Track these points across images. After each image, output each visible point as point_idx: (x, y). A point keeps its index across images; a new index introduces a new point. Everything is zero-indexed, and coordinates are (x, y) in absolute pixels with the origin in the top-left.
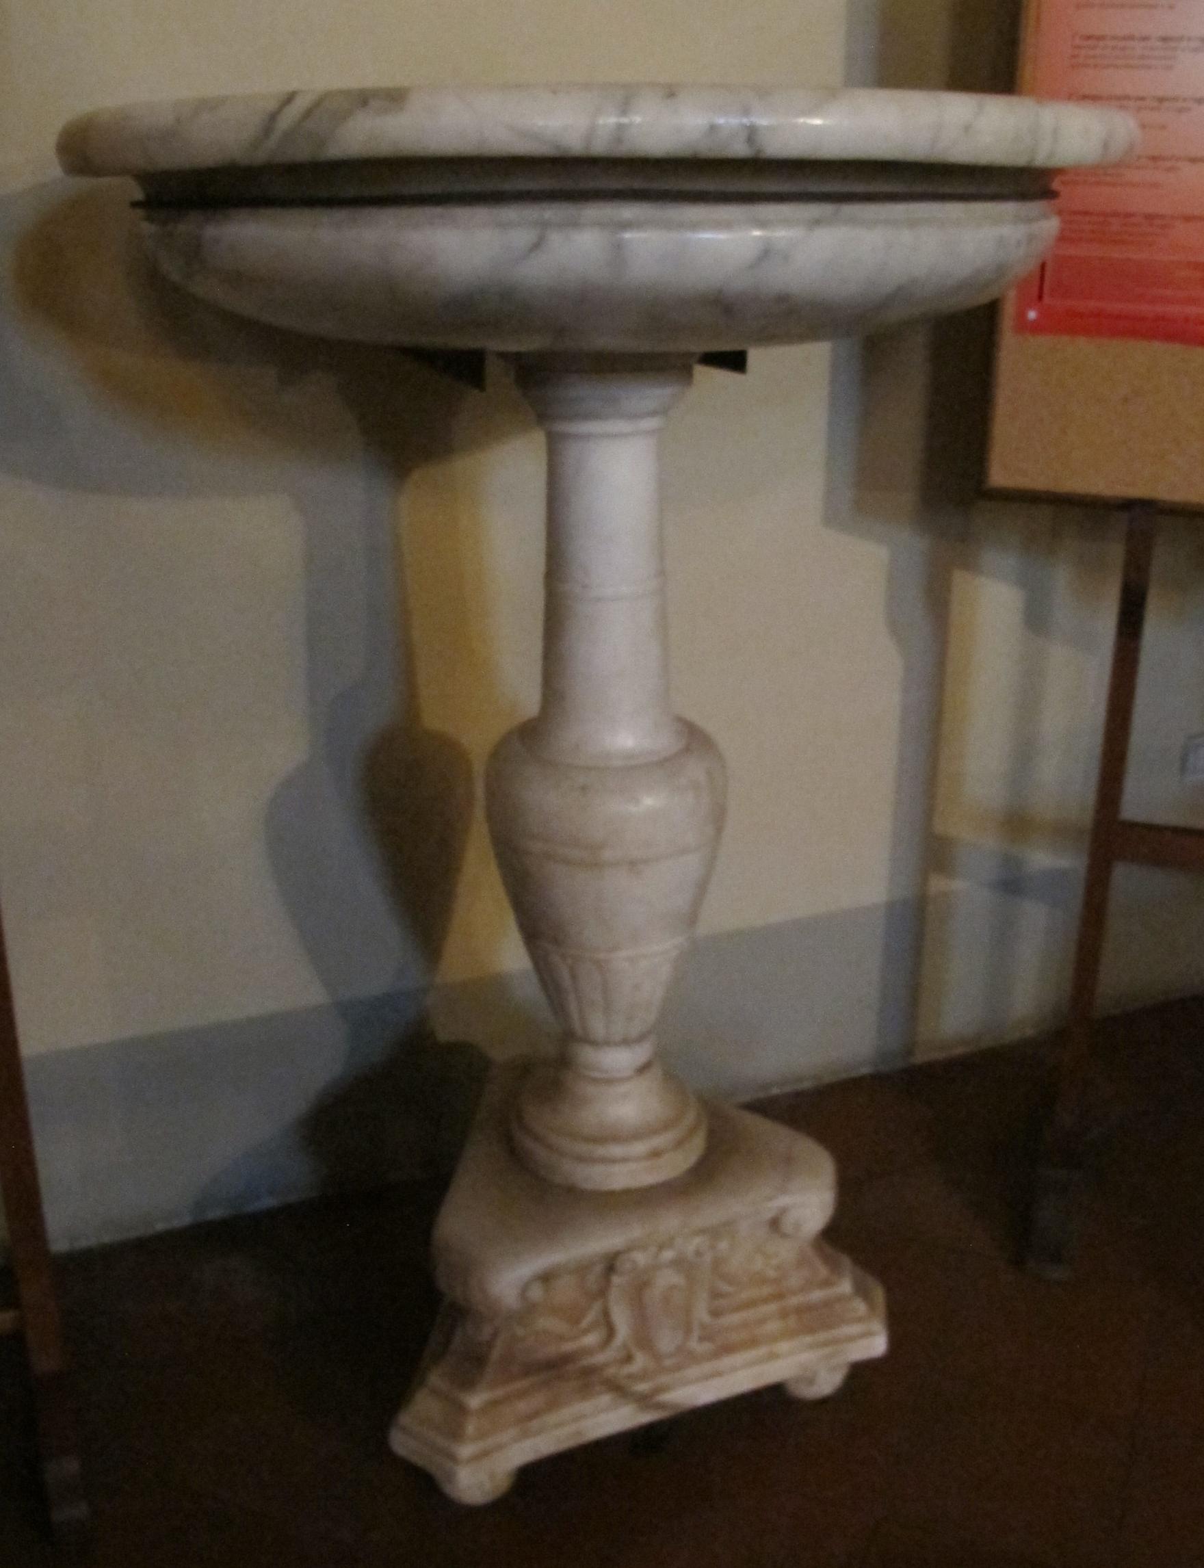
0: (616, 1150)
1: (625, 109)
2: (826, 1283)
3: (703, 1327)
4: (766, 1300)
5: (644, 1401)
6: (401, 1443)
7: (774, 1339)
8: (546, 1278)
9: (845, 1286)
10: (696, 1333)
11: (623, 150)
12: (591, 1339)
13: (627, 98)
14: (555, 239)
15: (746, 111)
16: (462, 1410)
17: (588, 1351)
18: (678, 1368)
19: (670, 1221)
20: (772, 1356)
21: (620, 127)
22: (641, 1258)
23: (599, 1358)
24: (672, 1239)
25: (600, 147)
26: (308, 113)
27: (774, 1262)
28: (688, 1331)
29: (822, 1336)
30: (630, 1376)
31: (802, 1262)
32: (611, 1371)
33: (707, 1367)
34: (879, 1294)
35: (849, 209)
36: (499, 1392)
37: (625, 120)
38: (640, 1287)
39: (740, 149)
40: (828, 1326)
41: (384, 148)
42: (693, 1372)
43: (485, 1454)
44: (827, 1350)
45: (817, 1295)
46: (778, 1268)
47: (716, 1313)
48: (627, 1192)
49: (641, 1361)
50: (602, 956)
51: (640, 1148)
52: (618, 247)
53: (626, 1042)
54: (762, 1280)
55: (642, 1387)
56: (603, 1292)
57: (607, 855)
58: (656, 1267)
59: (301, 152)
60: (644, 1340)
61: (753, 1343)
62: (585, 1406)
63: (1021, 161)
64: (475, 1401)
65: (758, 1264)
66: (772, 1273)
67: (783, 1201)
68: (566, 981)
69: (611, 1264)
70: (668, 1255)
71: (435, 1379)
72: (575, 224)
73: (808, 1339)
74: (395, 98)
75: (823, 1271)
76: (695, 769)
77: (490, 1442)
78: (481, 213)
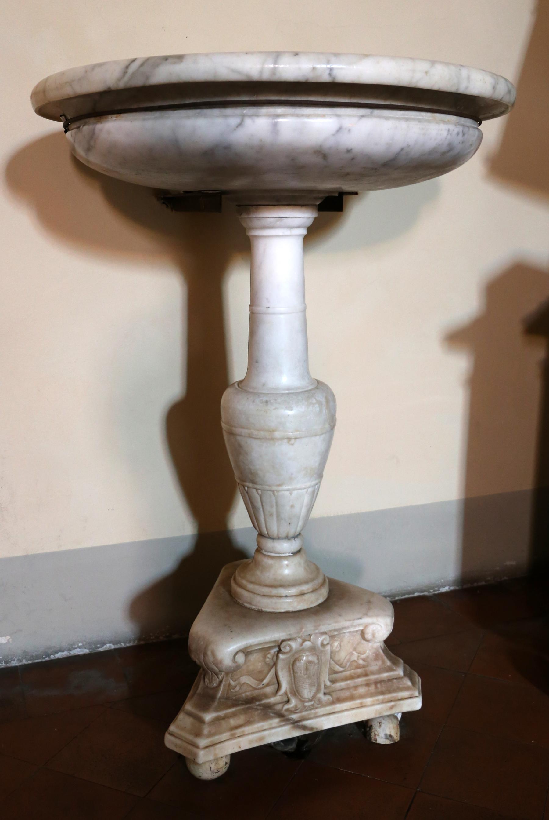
0: (283, 592)
1: (275, 62)
2: (390, 670)
3: (326, 687)
4: (359, 676)
5: (295, 724)
6: (170, 741)
7: (362, 697)
8: (246, 652)
9: (400, 672)
10: (323, 690)
11: (275, 78)
12: (269, 690)
13: (277, 56)
14: (248, 122)
15: (328, 62)
16: (201, 721)
17: (266, 696)
18: (313, 707)
19: (309, 626)
20: (362, 706)
21: (275, 69)
22: (294, 645)
23: (272, 700)
24: (310, 635)
25: (266, 77)
26: (142, 65)
27: (363, 656)
28: (318, 691)
29: (388, 696)
30: (287, 710)
31: (377, 657)
32: (279, 707)
33: (329, 709)
34: (418, 680)
35: (377, 112)
36: (222, 713)
37: (276, 66)
38: (292, 665)
39: (325, 78)
40: (390, 692)
41: (174, 79)
42: (321, 711)
43: (213, 745)
44: (392, 704)
45: (385, 675)
46: (364, 660)
47: (333, 681)
48: (287, 612)
49: (294, 702)
50: (274, 488)
51: (293, 591)
52: (275, 125)
53: (287, 538)
54: (358, 667)
55: (294, 717)
56: (275, 664)
57: (277, 434)
58: (301, 651)
59: (139, 82)
60: (295, 691)
61: (352, 698)
62: (265, 724)
63: (453, 89)
64: (208, 717)
65: (355, 657)
66: (361, 662)
67: (366, 620)
68: (259, 505)
69: (279, 646)
70: (308, 644)
71: (188, 706)
72: (257, 116)
73: (381, 697)
74: (180, 58)
75: (388, 663)
76: (320, 397)
77: (216, 738)
78: (216, 111)
